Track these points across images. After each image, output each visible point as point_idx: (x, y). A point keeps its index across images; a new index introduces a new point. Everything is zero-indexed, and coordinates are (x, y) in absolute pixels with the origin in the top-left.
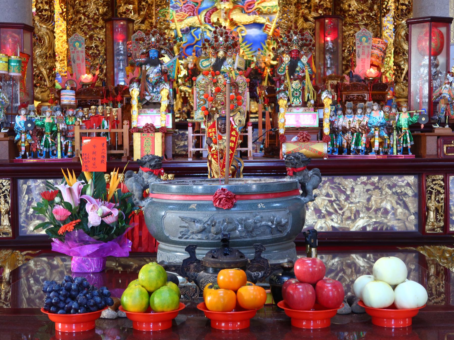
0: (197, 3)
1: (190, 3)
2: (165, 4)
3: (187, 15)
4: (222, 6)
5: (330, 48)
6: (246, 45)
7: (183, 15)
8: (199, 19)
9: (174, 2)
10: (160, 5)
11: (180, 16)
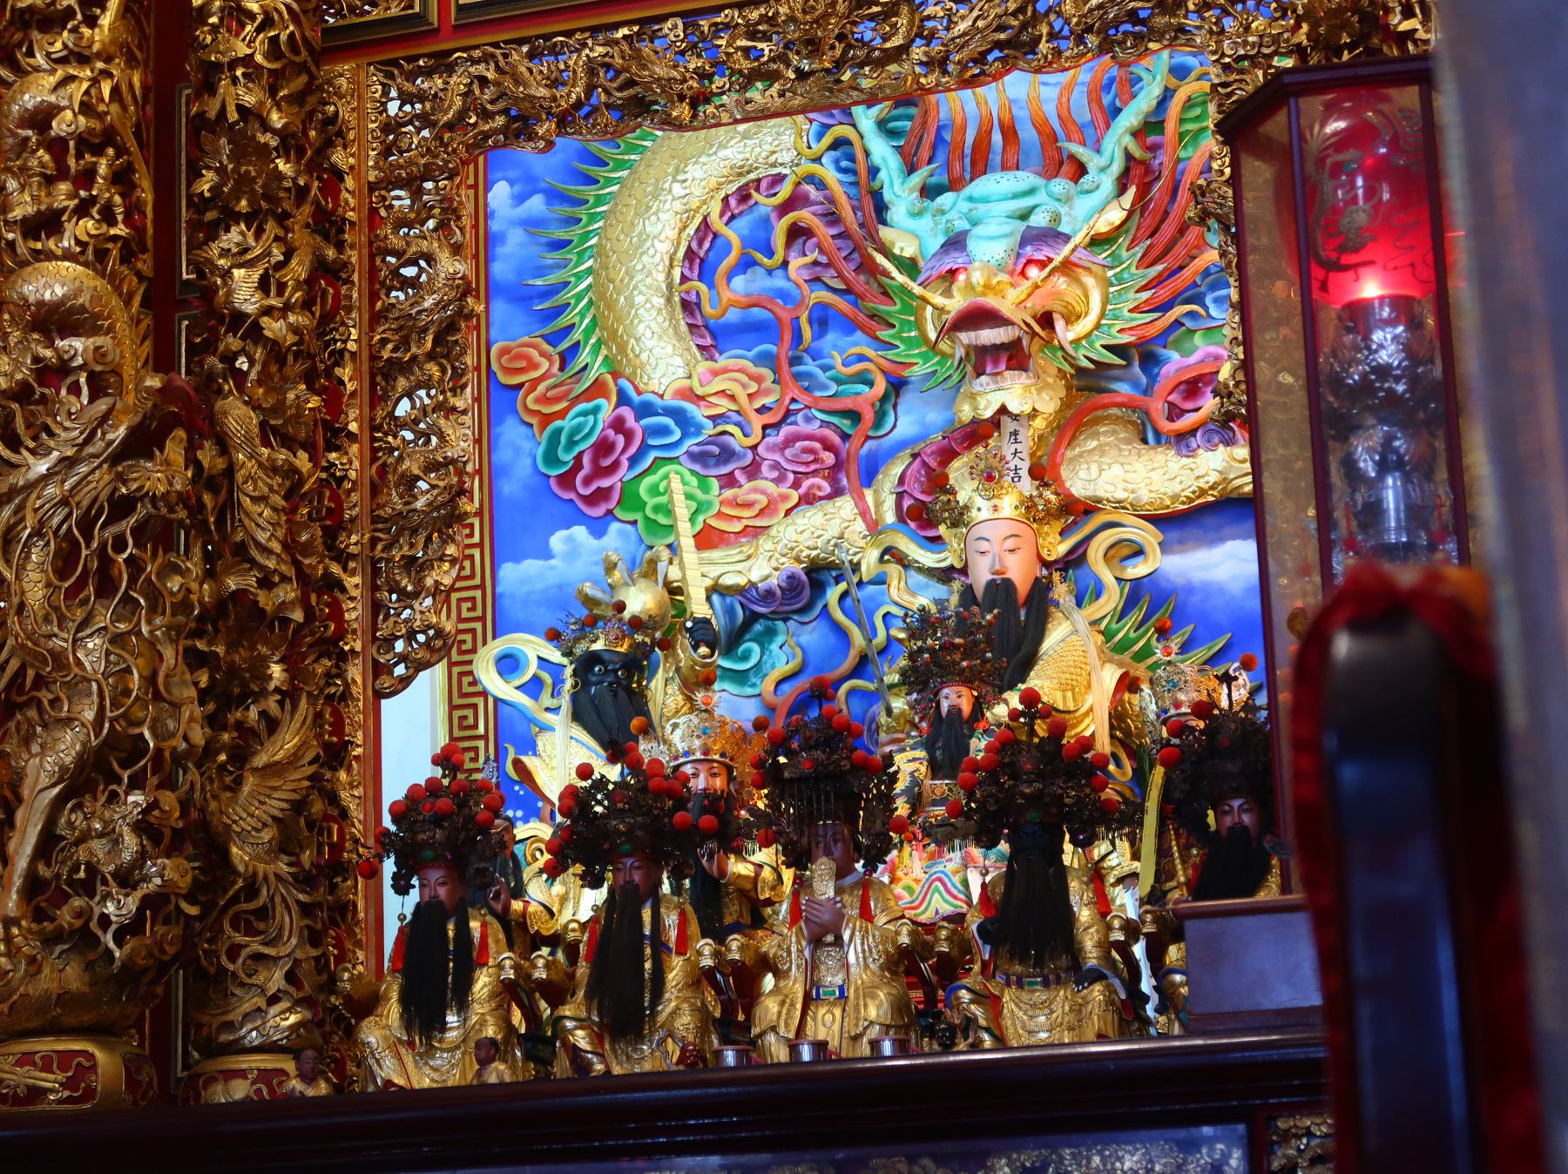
0: (854, 416)
1: (808, 419)
2: (431, 356)
3: (795, 496)
4: (982, 402)
5: (1383, 371)
6: (1185, 648)
7: (764, 500)
8: (864, 513)
9: (709, 423)
10: (405, 368)
11: (748, 505)
